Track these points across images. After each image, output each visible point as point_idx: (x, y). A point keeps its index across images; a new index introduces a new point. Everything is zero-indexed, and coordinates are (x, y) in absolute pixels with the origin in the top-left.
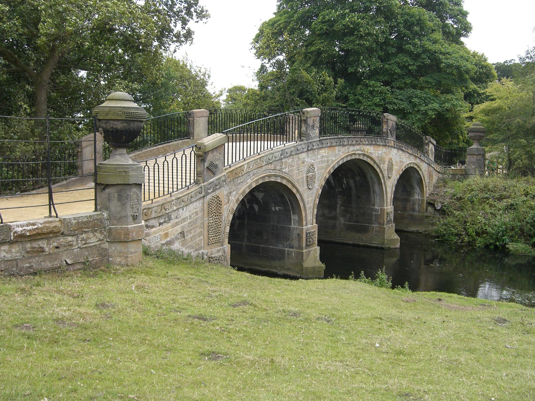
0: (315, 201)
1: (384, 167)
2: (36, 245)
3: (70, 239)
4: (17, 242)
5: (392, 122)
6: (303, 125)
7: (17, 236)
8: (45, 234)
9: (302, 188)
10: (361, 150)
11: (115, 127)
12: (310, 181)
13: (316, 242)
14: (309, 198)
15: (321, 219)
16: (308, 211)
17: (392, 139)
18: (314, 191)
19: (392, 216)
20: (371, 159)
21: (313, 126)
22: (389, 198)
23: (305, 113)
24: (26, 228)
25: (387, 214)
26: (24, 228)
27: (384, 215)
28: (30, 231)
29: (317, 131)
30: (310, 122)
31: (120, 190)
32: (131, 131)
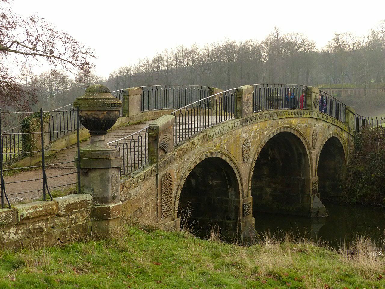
0: (258, 148)
1: (309, 139)
2: (37, 225)
3: (63, 219)
4: (23, 224)
5: (315, 94)
6: (238, 102)
7: (23, 219)
8: (44, 216)
9: (239, 161)
10: (288, 124)
11: (97, 117)
12: (244, 155)
13: (252, 213)
14: (245, 170)
15: (255, 191)
16: (245, 185)
17: (316, 111)
18: (248, 164)
19: (317, 185)
20: (298, 132)
21: (247, 102)
22: (314, 171)
23: (310, 89)
24: (30, 211)
25: (313, 183)
26: (28, 211)
27: (310, 188)
28: (33, 213)
29: (251, 108)
30: (245, 99)
31: (102, 174)
32: (110, 120)
